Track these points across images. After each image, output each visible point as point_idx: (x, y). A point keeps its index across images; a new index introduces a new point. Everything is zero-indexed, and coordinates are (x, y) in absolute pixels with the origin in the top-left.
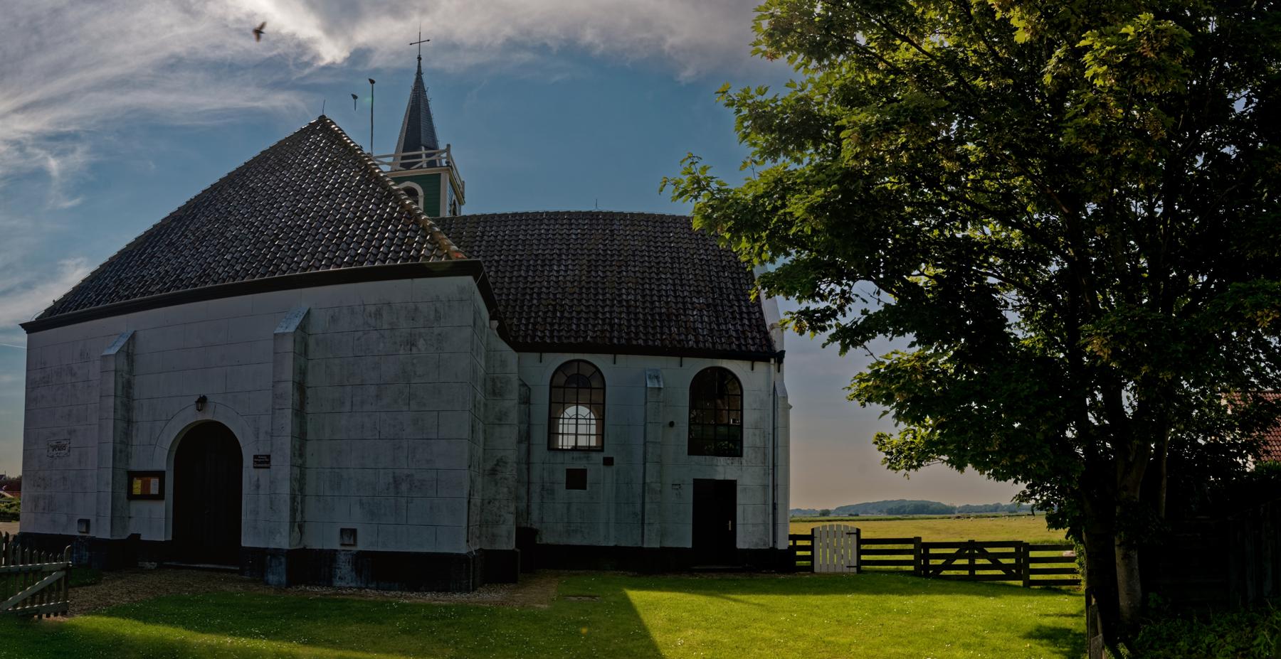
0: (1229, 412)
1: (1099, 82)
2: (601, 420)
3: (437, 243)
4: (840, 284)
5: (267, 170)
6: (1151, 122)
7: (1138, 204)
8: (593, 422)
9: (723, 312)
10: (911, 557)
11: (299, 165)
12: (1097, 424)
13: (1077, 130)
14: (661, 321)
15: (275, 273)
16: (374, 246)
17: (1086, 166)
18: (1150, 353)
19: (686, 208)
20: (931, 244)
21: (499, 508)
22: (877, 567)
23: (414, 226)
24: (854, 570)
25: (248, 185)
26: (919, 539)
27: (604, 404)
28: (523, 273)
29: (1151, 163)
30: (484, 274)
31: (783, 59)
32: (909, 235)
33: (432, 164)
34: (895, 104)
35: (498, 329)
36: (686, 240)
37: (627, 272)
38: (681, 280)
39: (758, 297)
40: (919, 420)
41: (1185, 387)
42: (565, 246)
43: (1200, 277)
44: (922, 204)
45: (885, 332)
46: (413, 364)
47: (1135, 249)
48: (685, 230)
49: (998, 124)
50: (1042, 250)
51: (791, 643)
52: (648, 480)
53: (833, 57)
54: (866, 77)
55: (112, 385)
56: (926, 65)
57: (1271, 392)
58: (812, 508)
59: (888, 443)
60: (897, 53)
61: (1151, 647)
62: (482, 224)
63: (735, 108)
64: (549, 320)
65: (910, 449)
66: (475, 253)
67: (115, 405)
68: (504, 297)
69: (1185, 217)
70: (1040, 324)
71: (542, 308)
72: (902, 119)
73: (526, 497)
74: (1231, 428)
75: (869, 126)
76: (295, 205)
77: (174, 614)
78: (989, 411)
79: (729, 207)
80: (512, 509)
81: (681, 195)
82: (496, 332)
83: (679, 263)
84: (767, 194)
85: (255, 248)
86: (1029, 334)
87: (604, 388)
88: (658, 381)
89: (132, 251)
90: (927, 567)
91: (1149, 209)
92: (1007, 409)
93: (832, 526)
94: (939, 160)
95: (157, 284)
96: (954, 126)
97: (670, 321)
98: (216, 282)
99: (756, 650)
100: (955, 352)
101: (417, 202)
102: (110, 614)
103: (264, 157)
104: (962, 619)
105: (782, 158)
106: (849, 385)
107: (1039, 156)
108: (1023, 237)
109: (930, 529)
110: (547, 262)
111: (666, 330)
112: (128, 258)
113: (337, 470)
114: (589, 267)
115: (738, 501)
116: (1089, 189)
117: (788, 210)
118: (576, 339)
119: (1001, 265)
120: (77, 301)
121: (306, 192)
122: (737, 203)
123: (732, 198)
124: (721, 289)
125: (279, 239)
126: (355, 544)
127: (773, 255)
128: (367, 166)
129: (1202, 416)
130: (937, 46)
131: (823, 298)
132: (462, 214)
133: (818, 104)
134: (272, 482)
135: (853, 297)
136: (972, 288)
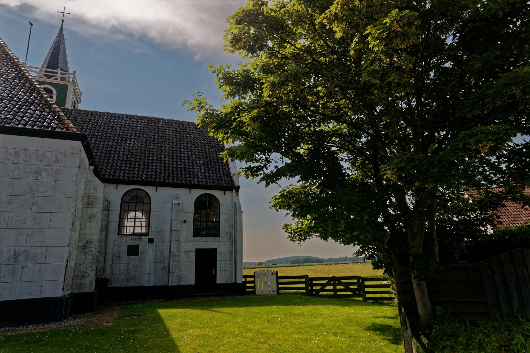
0: (471, 201)
1: (376, 49)
2: (148, 219)
4: (264, 154)
6: (404, 62)
7: (403, 103)
8: (144, 220)
10: (304, 286)
12: (394, 214)
13: (368, 74)
14: (181, 171)
17: (374, 90)
18: (419, 175)
20: (305, 134)
21: (86, 268)
26: (307, 276)
29: (407, 81)
31: (237, 53)
32: (294, 131)
34: (286, 73)
35: (93, 170)
39: (227, 161)
40: (304, 217)
41: (441, 190)
43: (441, 133)
44: (300, 117)
45: (286, 176)
47: (404, 125)
49: (332, 77)
50: (357, 132)
52: (172, 250)
53: (258, 52)
54: (273, 61)
56: (298, 54)
57: (497, 188)
58: (254, 261)
59: (290, 228)
60: (286, 50)
61: (441, 339)
63: (216, 74)
64: (123, 168)
65: (301, 231)
69: (428, 104)
70: (359, 167)
71: (120, 161)
72: (289, 79)
73: (103, 261)
74: (473, 210)
75: (275, 83)
78: (338, 210)
80: (94, 268)
82: (92, 172)
86: (354, 173)
87: (150, 203)
88: (179, 200)
90: (312, 290)
91: (409, 104)
92: (347, 209)
94: (306, 96)
96: (312, 80)
97: (185, 171)
100: (320, 184)
104: (332, 319)
105: (237, 97)
106: (270, 201)
107: (351, 89)
108: (348, 127)
109: (312, 270)
111: (184, 176)
115: (217, 259)
116: (377, 100)
118: (137, 177)
119: (338, 141)
129: (453, 206)
130: (302, 44)
131: (257, 161)
133: (253, 73)
135: (271, 160)
136: (326, 153)
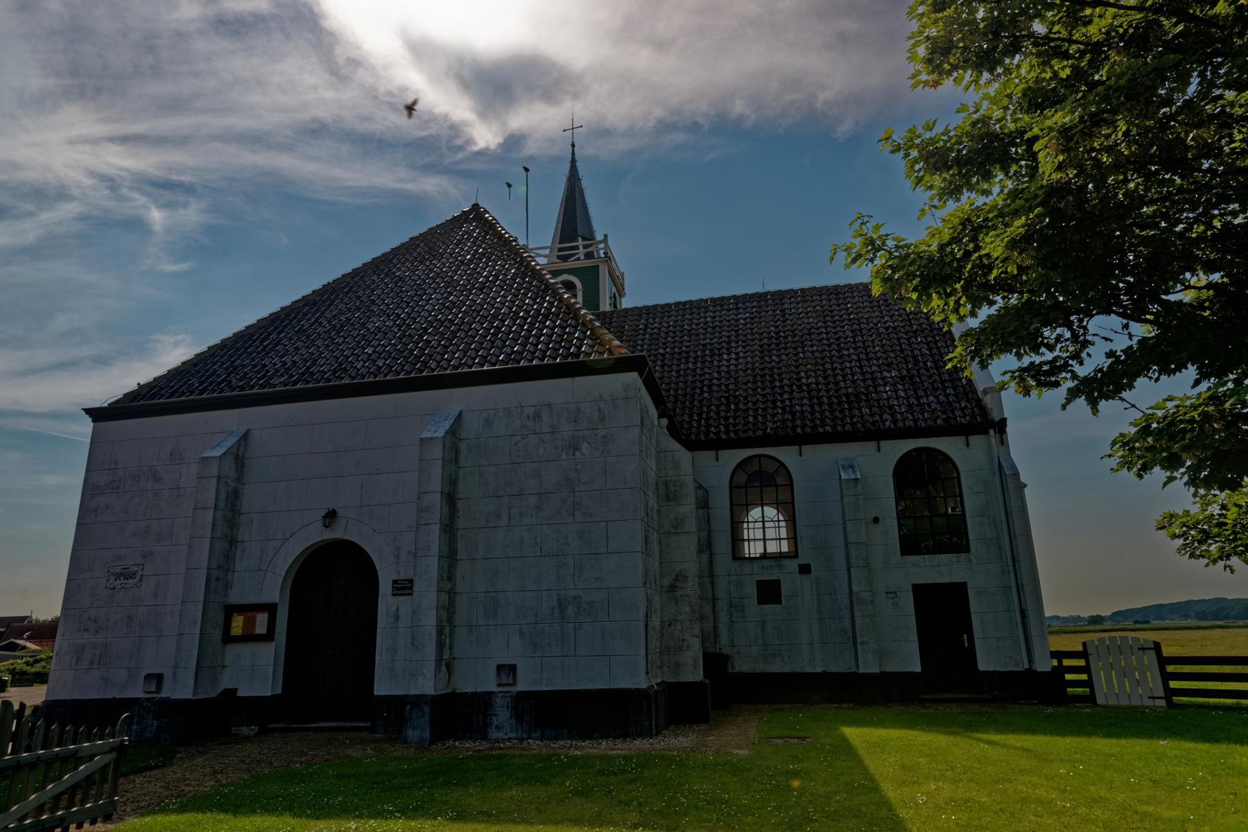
3: (598, 338)
5: (416, 258)
8: (783, 524)
9: (922, 382)
11: (451, 255)
14: (849, 403)
15: (422, 371)
16: (531, 343)
19: (862, 274)
22: (1201, 700)
23: (573, 321)
24: (1163, 703)
25: (394, 273)
27: (793, 503)
28: (690, 365)
30: (650, 370)
33: (589, 256)
35: (668, 428)
36: (867, 309)
37: (804, 353)
38: (867, 354)
42: (733, 333)
46: (577, 470)
48: (865, 298)
51: (1082, 810)
52: (855, 589)
55: (212, 494)
58: (1075, 614)
62: (644, 316)
64: (722, 414)
66: (639, 348)
67: (214, 519)
68: (672, 392)
76: (446, 298)
77: (278, 796)
79: (911, 264)
80: (697, 631)
81: (854, 260)
82: (666, 431)
83: (862, 336)
84: (955, 240)
85: (400, 343)
88: (854, 472)
89: (252, 335)
93: (1110, 638)
95: (282, 375)
98: (353, 378)
99: (1032, 817)
101: (575, 296)
102: (182, 809)
103: (413, 243)
106: (1110, 452)
110: (716, 352)
112: (246, 342)
113: (493, 594)
114: (762, 352)
117: (983, 252)
118: (754, 432)
120: (172, 387)
121: (458, 285)
122: (921, 258)
123: (914, 253)
124: (915, 357)
125: (427, 334)
126: (514, 684)
127: (974, 307)
128: (522, 258)
132: (623, 307)
134: (414, 612)
135: (1089, 338)
